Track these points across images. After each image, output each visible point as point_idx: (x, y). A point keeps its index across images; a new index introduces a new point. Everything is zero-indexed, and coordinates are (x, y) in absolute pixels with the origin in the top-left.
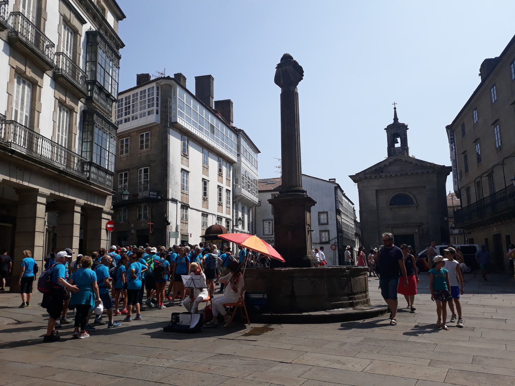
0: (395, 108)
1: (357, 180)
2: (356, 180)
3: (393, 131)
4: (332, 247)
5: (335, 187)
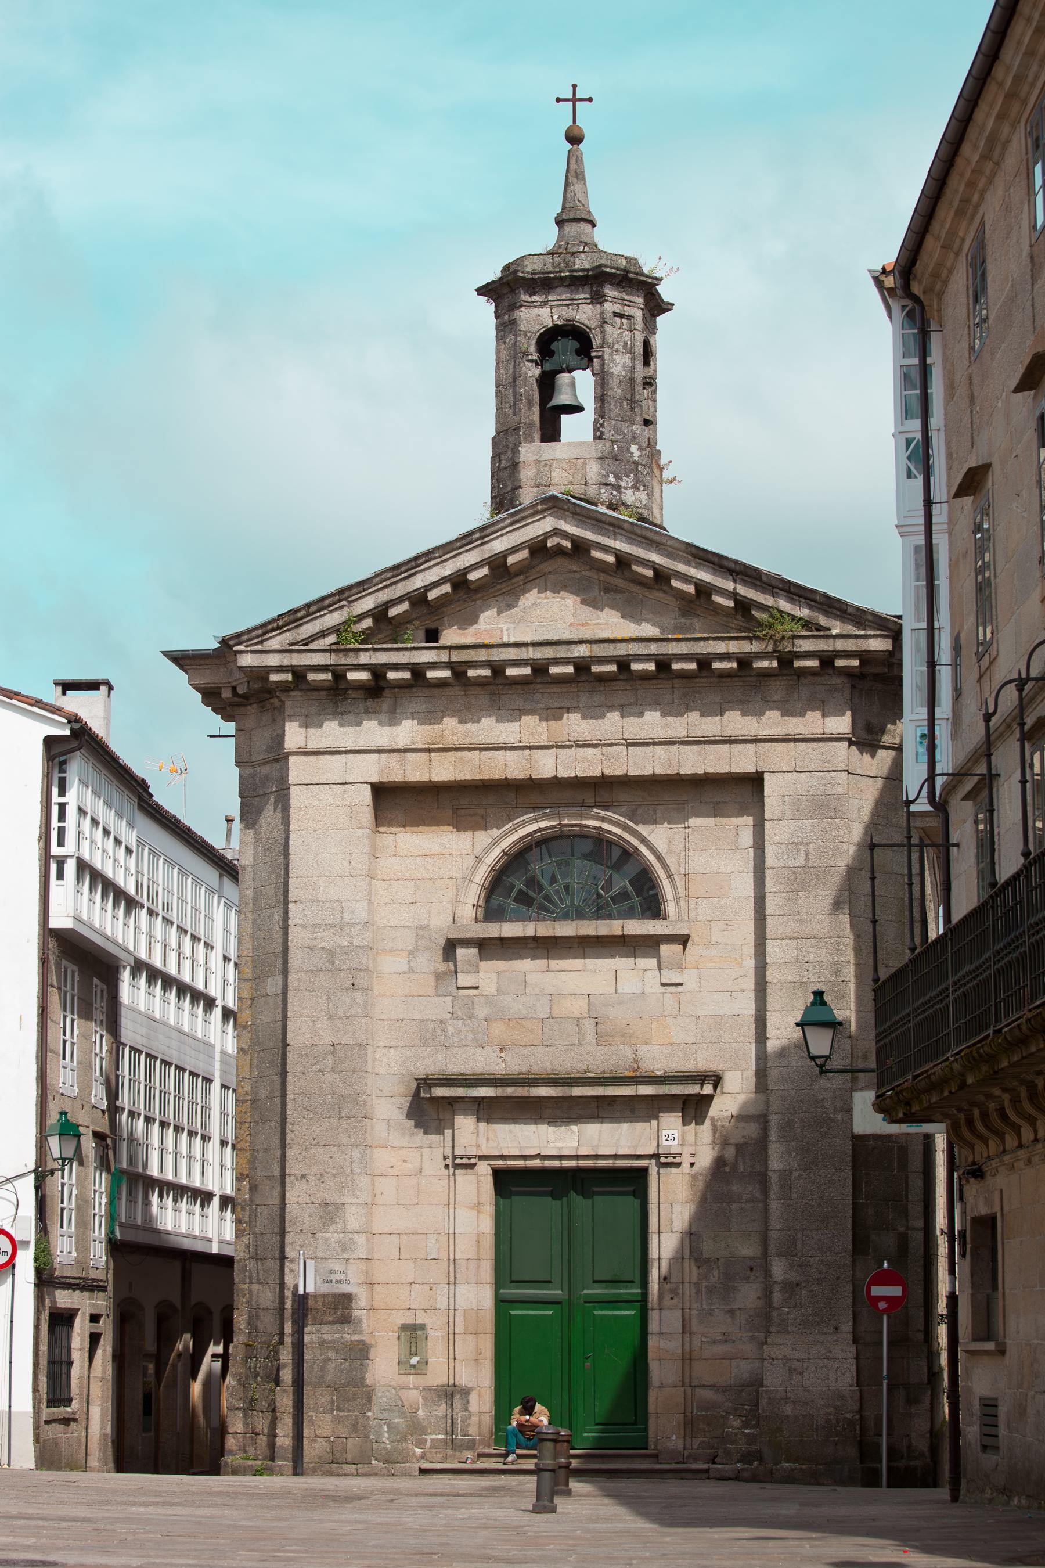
0: (574, 138)
1: (234, 689)
2: (226, 694)
3: (546, 311)
5: (49, 742)
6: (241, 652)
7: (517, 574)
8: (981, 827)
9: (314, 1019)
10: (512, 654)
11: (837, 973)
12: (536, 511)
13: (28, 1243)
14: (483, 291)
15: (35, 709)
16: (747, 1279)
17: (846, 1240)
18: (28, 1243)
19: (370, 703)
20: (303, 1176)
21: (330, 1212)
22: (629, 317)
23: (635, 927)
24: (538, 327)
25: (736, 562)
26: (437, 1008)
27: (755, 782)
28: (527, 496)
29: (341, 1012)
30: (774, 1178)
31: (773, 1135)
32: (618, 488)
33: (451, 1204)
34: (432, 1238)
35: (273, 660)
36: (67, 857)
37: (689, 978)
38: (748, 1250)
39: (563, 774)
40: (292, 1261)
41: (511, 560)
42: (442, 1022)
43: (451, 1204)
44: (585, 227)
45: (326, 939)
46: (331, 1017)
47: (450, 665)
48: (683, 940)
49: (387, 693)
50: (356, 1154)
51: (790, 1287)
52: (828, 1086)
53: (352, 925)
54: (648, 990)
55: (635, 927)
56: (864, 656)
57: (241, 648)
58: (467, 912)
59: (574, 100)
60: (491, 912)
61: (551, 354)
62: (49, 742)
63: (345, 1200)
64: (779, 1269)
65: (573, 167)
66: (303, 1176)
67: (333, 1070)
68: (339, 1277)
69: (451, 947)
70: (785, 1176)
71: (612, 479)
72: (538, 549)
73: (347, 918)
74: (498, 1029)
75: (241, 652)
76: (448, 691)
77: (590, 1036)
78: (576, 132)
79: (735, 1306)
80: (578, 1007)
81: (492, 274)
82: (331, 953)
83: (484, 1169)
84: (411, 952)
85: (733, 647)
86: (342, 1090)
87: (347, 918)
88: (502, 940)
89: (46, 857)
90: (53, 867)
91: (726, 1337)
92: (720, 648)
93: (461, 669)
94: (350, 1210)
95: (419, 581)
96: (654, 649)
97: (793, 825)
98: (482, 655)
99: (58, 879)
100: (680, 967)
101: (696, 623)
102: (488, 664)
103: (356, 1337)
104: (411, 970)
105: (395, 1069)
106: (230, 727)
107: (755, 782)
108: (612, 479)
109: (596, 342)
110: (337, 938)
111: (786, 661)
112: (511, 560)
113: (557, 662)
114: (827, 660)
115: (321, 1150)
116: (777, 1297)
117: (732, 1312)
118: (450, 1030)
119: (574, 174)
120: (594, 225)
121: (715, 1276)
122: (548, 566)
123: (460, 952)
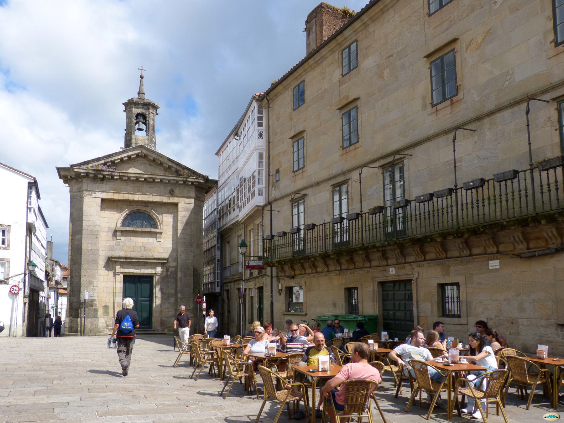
2: (69, 177)
4: (12, 290)
6: (75, 168)
7: (133, 160)
8: (472, 184)
9: (88, 244)
10: (132, 175)
11: (191, 241)
12: (134, 149)
13: (22, 288)
14: (124, 104)
15: (26, 176)
16: (172, 297)
17: (192, 290)
18: (22, 288)
19: (101, 182)
20: (85, 275)
21: (91, 283)
22: (153, 114)
23: (153, 230)
24: (136, 112)
25: (177, 162)
26: (112, 243)
27: (176, 205)
28: (133, 145)
29: (93, 243)
30: (179, 278)
31: (179, 270)
32: (151, 146)
33: (115, 282)
34: (110, 288)
35: (82, 171)
36: (32, 208)
37: (162, 240)
38: (172, 291)
39: (140, 199)
40: (82, 292)
41: (132, 157)
42: (113, 246)
43: (115, 282)
44: (144, 95)
45: (91, 228)
46: (91, 244)
47: (120, 176)
48: (161, 233)
49: (105, 180)
50: (96, 271)
51: (181, 299)
52: (189, 261)
53: (96, 226)
54: (154, 242)
55: (153, 230)
56: (199, 183)
57: (75, 167)
58: (119, 225)
59: (142, 70)
60: (123, 224)
61: (138, 118)
62: (29, 183)
63: (94, 280)
64: (179, 295)
65: (141, 83)
66: (85, 275)
67: (92, 254)
68: (93, 296)
69: (115, 231)
70: (181, 278)
71: (150, 144)
72: (137, 155)
73: (95, 224)
74: (125, 248)
75: (75, 168)
76: (118, 181)
77: (143, 250)
78: (142, 76)
79: (170, 302)
80: (141, 244)
81: (126, 101)
82: (92, 231)
83: (122, 275)
84: (107, 232)
85: (176, 178)
86: (94, 258)
87: (95, 224)
88: (126, 231)
89: (28, 208)
90: (29, 210)
91: (168, 308)
92: (173, 178)
93: (122, 177)
94: (95, 282)
95: (114, 159)
96: (160, 177)
97: (184, 213)
98: (126, 175)
99: (103, 200)
100: (160, 238)
101: (167, 173)
102: (127, 176)
103: (95, 308)
104: (107, 235)
105: (104, 255)
106: (67, 185)
107: (176, 205)
108: (150, 144)
109: (148, 117)
110: (93, 228)
111: (185, 182)
112: (132, 157)
113: (141, 177)
114: (192, 183)
115: (89, 270)
116: (179, 301)
117: (169, 303)
118: (115, 248)
119: (141, 85)
120: (145, 94)
121: (166, 296)
122: (138, 159)
123: (118, 233)
